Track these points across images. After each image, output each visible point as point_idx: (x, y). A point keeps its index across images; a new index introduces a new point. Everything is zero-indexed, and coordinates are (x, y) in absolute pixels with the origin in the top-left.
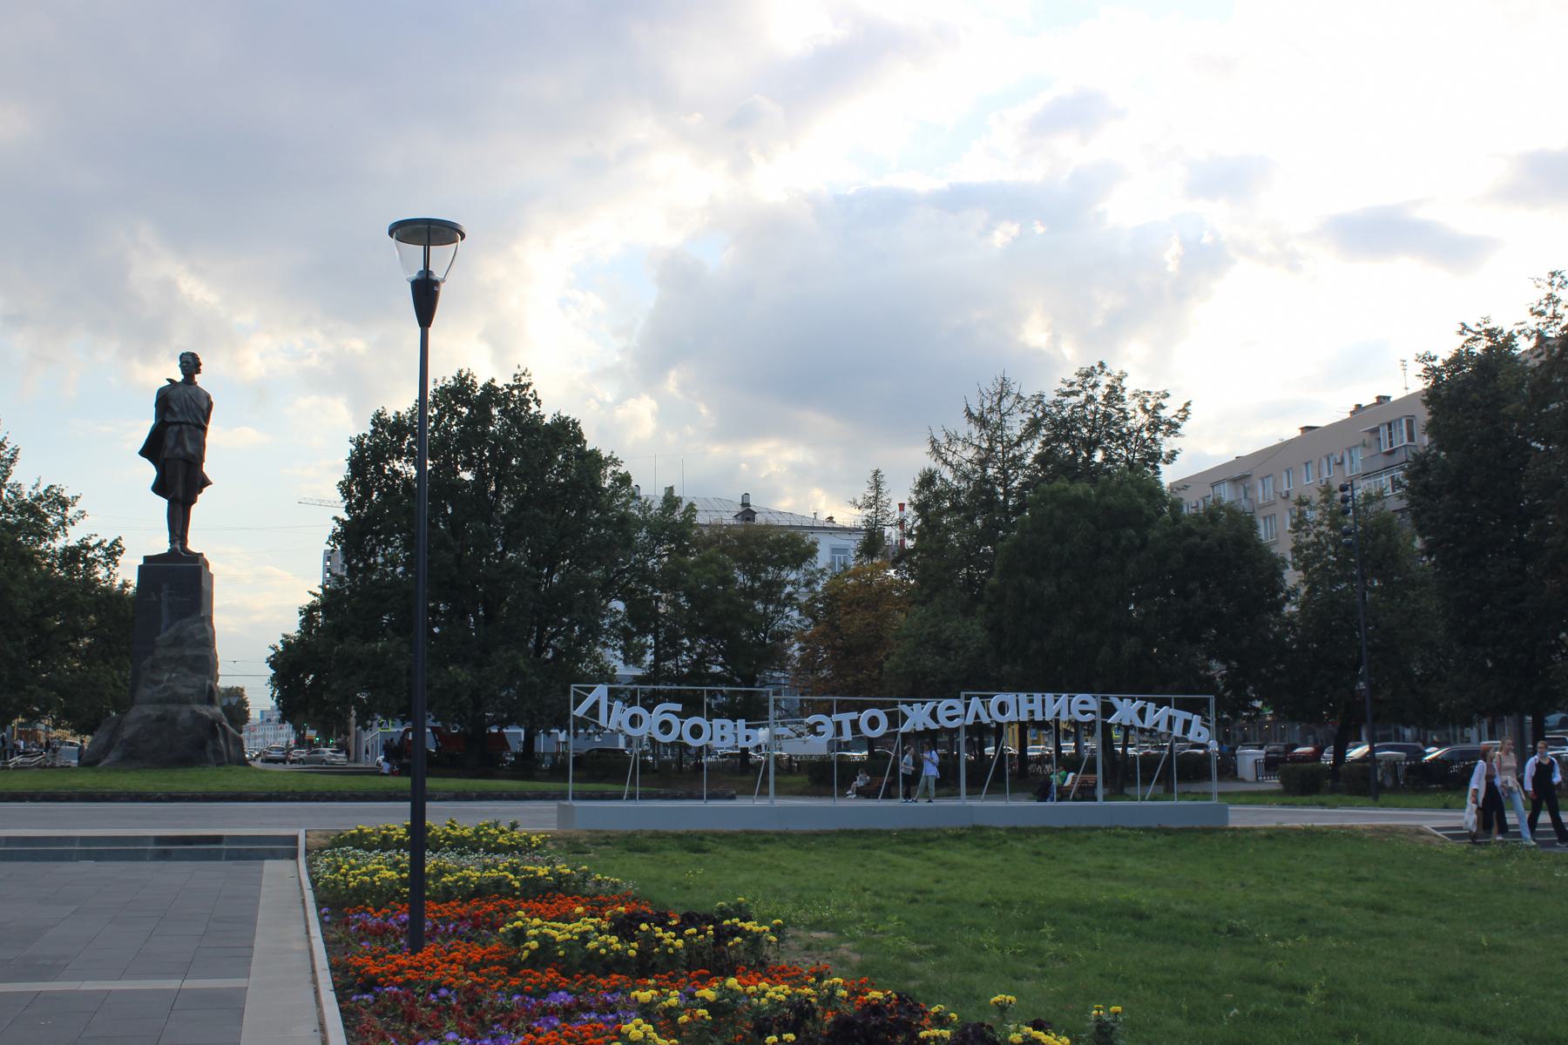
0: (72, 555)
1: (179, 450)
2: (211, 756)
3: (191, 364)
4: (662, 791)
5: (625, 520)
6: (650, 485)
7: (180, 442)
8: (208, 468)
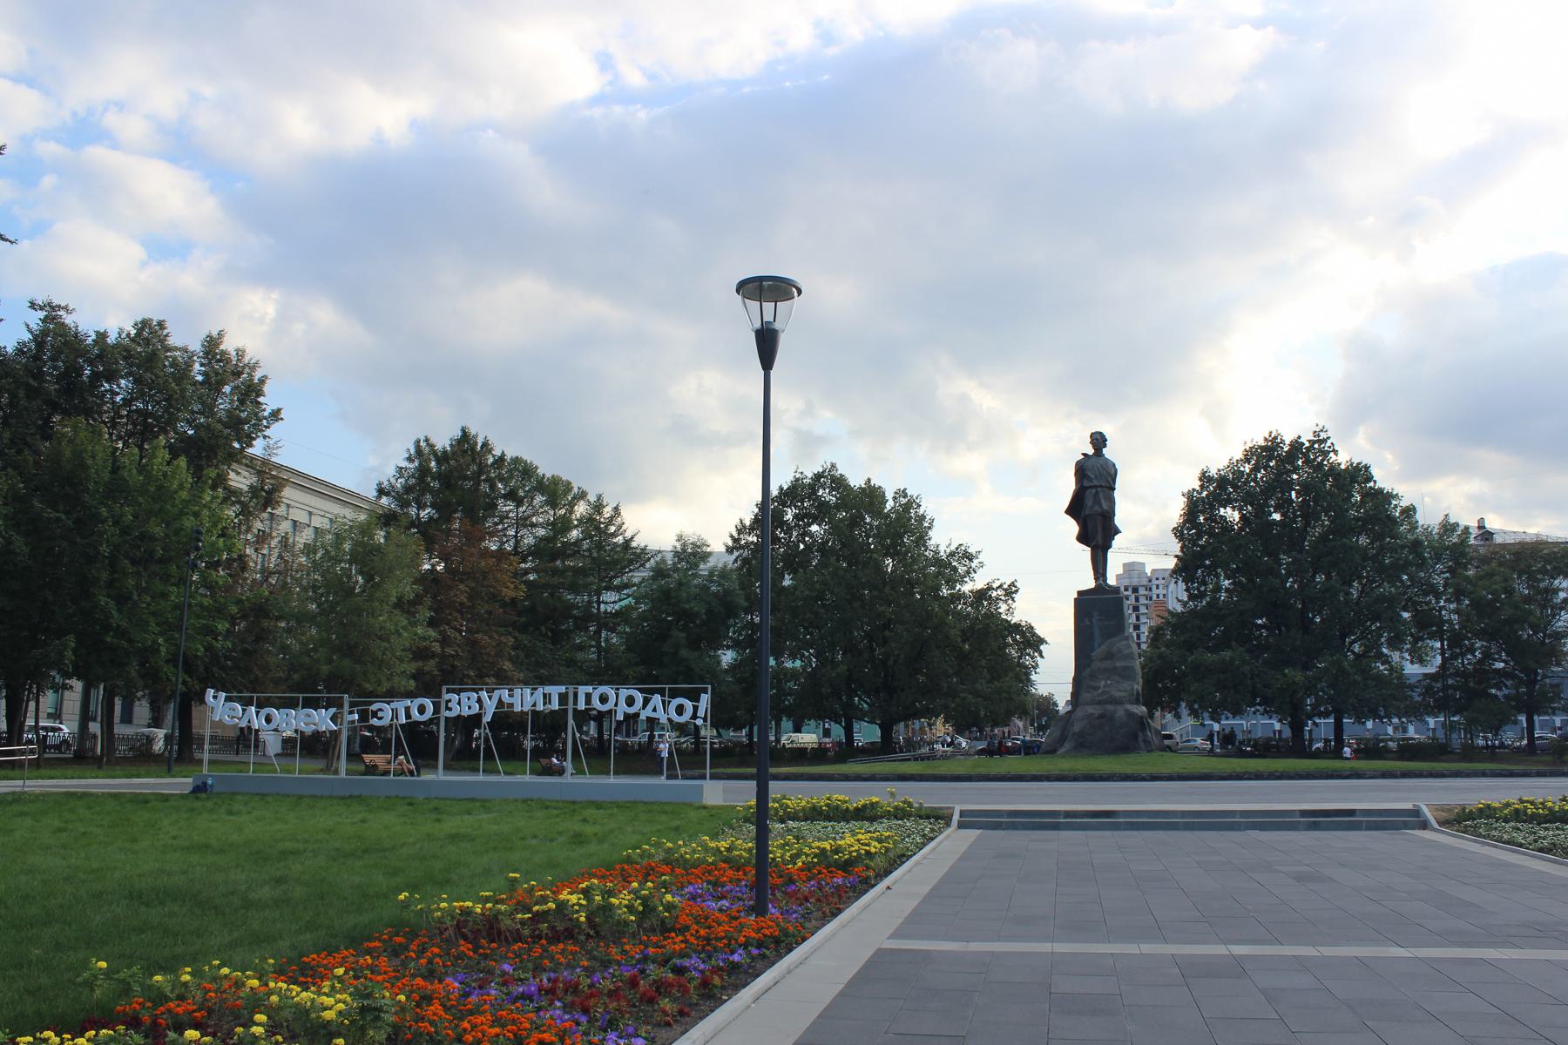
0: (982, 595)
1: (1096, 508)
2: (1142, 744)
3: (1099, 441)
4: (1534, 768)
5: (1417, 544)
6: (1428, 518)
7: (1097, 501)
8: (1119, 520)
